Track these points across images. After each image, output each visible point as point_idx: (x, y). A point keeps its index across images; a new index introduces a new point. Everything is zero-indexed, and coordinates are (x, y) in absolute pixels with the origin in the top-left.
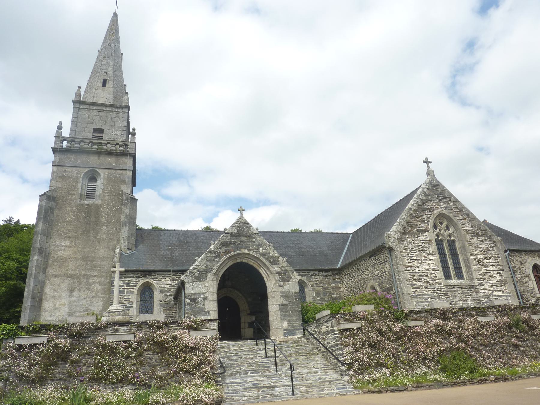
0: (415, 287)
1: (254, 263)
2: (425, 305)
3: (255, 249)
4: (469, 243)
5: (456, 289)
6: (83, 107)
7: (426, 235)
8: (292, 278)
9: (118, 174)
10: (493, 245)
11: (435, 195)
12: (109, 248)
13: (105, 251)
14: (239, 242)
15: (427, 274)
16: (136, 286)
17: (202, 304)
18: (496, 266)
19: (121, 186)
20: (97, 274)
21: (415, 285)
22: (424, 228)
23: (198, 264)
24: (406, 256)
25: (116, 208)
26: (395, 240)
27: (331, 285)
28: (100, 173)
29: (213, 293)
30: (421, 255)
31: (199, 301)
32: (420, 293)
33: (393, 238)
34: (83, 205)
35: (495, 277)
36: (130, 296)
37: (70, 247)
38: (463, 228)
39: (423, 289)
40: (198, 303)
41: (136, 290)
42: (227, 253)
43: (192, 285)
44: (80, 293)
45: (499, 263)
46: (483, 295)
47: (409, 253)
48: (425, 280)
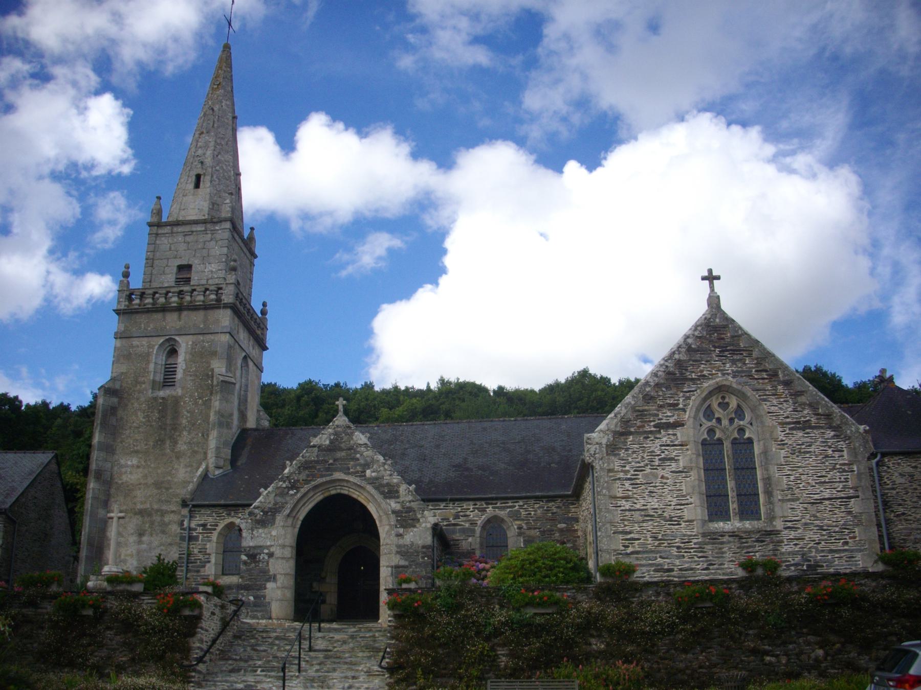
0: (629, 536)
1: (359, 496)
2: (644, 571)
3: (358, 472)
4: (779, 445)
5: (725, 539)
6: (163, 232)
7: (675, 435)
8: (421, 521)
9: (208, 342)
10: (842, 445)
11: (713, 349)
12: (192, 466)
13: (186, 472)
14: (331, 461)
15: (663, 512)
16: (215, 529)
17: (265, 563)
18: (839, 489)
19: (212, 362)
20: (174, 509)
21: (630, 533)
22: (672, 420)
23: (263, 500)
24: (619, 479)
25: (203, 401)
26: (601, 447)
27: (559, 526)
28: (181, 342)
29: (284, 546)
30: (656, 476)
31: (261, 558)
32: (639, 549)
33: (597, 444)
34: (155, 399)
35: (831, 513)
36: (206, 545)
37: (138, 467)
38: (769, 413)
39: (648, 540)
40: (259, 561)
41: (215, 536)
42: (311, 480)
43: (252, 534)
44: (152, 539)
45: (850, 483)
46: (790, 550)
47: (628, 471)
48: (656, 524)
